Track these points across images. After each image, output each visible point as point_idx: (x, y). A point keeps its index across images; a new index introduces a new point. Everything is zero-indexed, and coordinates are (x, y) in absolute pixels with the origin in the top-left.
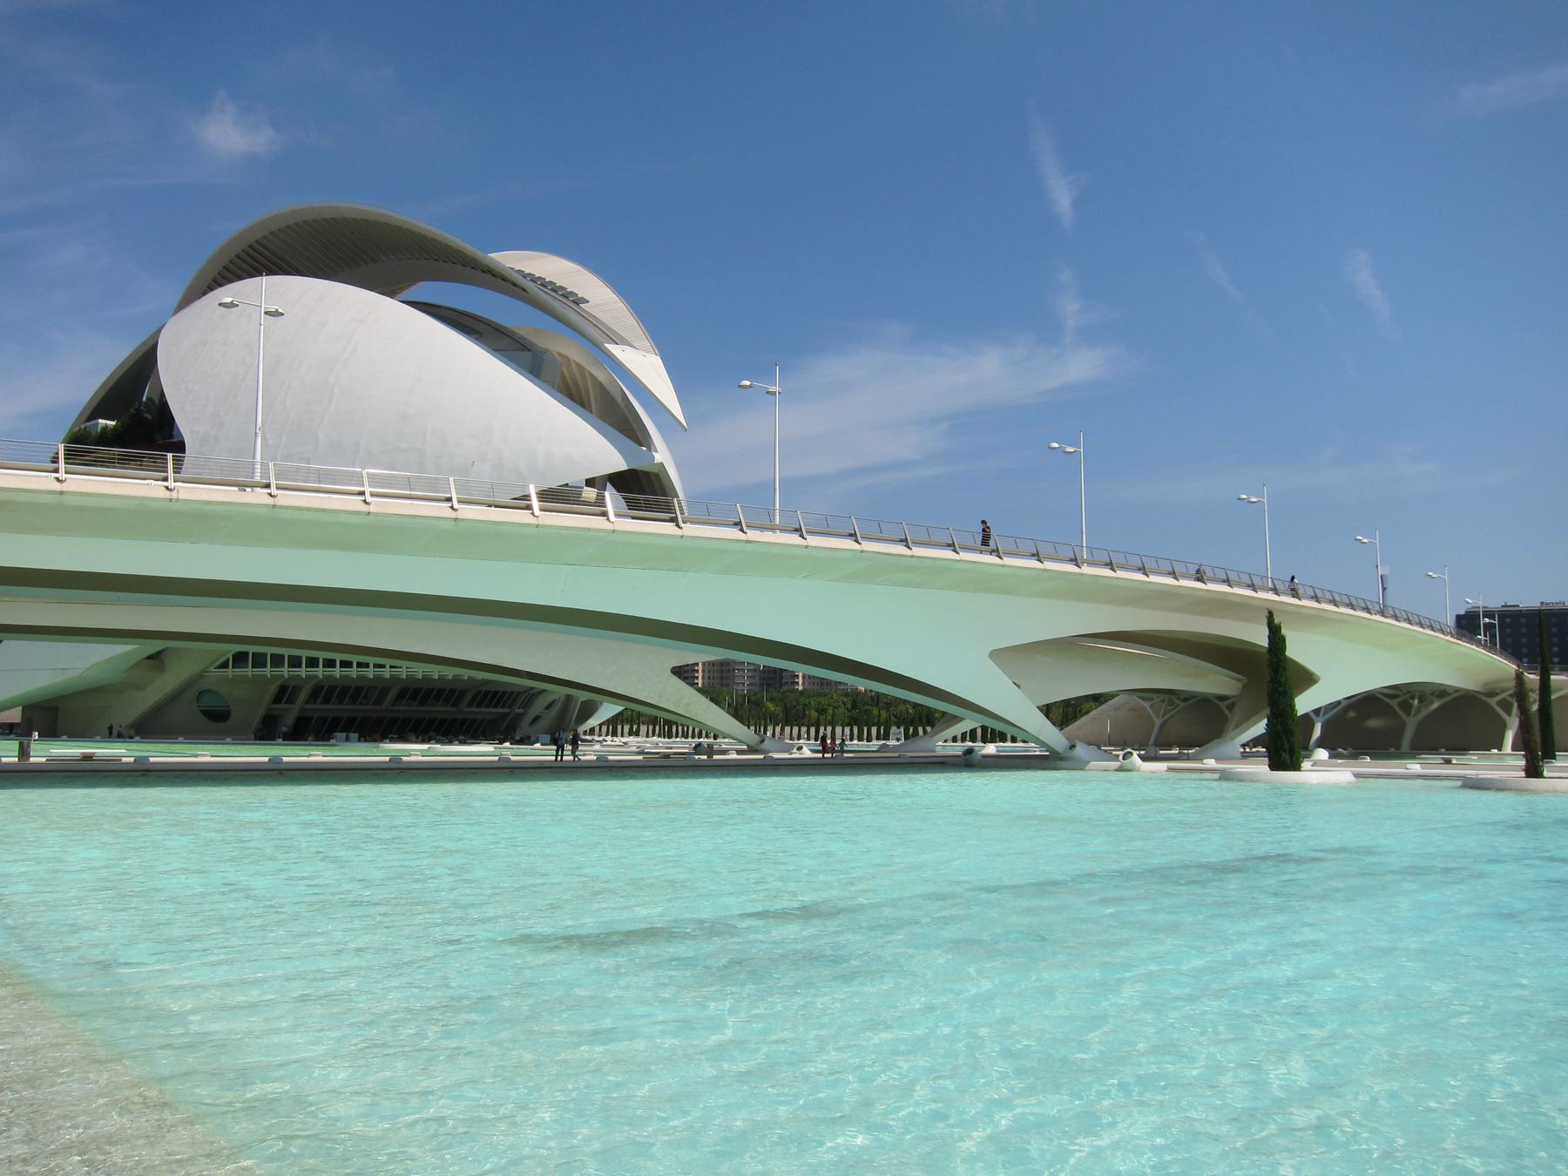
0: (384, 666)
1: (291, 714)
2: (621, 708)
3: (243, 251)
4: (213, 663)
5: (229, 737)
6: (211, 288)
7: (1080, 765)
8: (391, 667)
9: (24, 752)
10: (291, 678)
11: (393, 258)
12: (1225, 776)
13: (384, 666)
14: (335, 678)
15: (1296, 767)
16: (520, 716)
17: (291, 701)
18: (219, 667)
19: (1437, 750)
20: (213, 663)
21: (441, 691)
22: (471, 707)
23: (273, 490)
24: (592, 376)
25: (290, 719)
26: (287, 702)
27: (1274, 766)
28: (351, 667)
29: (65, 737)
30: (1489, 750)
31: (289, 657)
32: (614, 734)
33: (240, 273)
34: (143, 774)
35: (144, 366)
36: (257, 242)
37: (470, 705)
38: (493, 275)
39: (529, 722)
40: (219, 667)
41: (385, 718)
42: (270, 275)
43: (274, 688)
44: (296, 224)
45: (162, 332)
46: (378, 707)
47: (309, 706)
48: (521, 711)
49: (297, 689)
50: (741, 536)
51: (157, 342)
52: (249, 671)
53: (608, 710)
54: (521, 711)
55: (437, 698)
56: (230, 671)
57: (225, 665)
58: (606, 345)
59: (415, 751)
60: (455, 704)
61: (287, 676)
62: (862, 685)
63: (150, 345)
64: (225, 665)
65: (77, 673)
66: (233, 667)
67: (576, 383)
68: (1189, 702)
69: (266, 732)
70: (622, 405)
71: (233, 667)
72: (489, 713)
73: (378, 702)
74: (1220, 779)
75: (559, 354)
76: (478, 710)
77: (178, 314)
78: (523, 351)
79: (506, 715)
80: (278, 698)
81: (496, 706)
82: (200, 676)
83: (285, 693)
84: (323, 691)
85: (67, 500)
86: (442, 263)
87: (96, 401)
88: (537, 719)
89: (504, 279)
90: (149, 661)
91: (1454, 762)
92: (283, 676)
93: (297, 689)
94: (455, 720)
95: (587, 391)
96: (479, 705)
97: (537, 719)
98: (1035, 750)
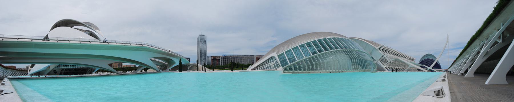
1: (63, 72)
2: (99, 69)
7: (160, 73)
9: (39, 77)
15: (181, 71)
17: (63, 71)
21: (67, 69)
25: (63, 73)
27: (180, 71)
32: (102, 73)
34: (362, 39)
38: (448, 38)
42: (495, 42)
43: (61, 70)
49: (64, 70)
50: (137, 45)
53: (97, 69)
56: (57, 68)
57: (56, 67)
59: (69, 76)
64: (56, 67)
69: (61, 74)
82: (53, 69)
83: (62, 70)
85: (70, 44)
89: (83, 24)
93: (64, 70)
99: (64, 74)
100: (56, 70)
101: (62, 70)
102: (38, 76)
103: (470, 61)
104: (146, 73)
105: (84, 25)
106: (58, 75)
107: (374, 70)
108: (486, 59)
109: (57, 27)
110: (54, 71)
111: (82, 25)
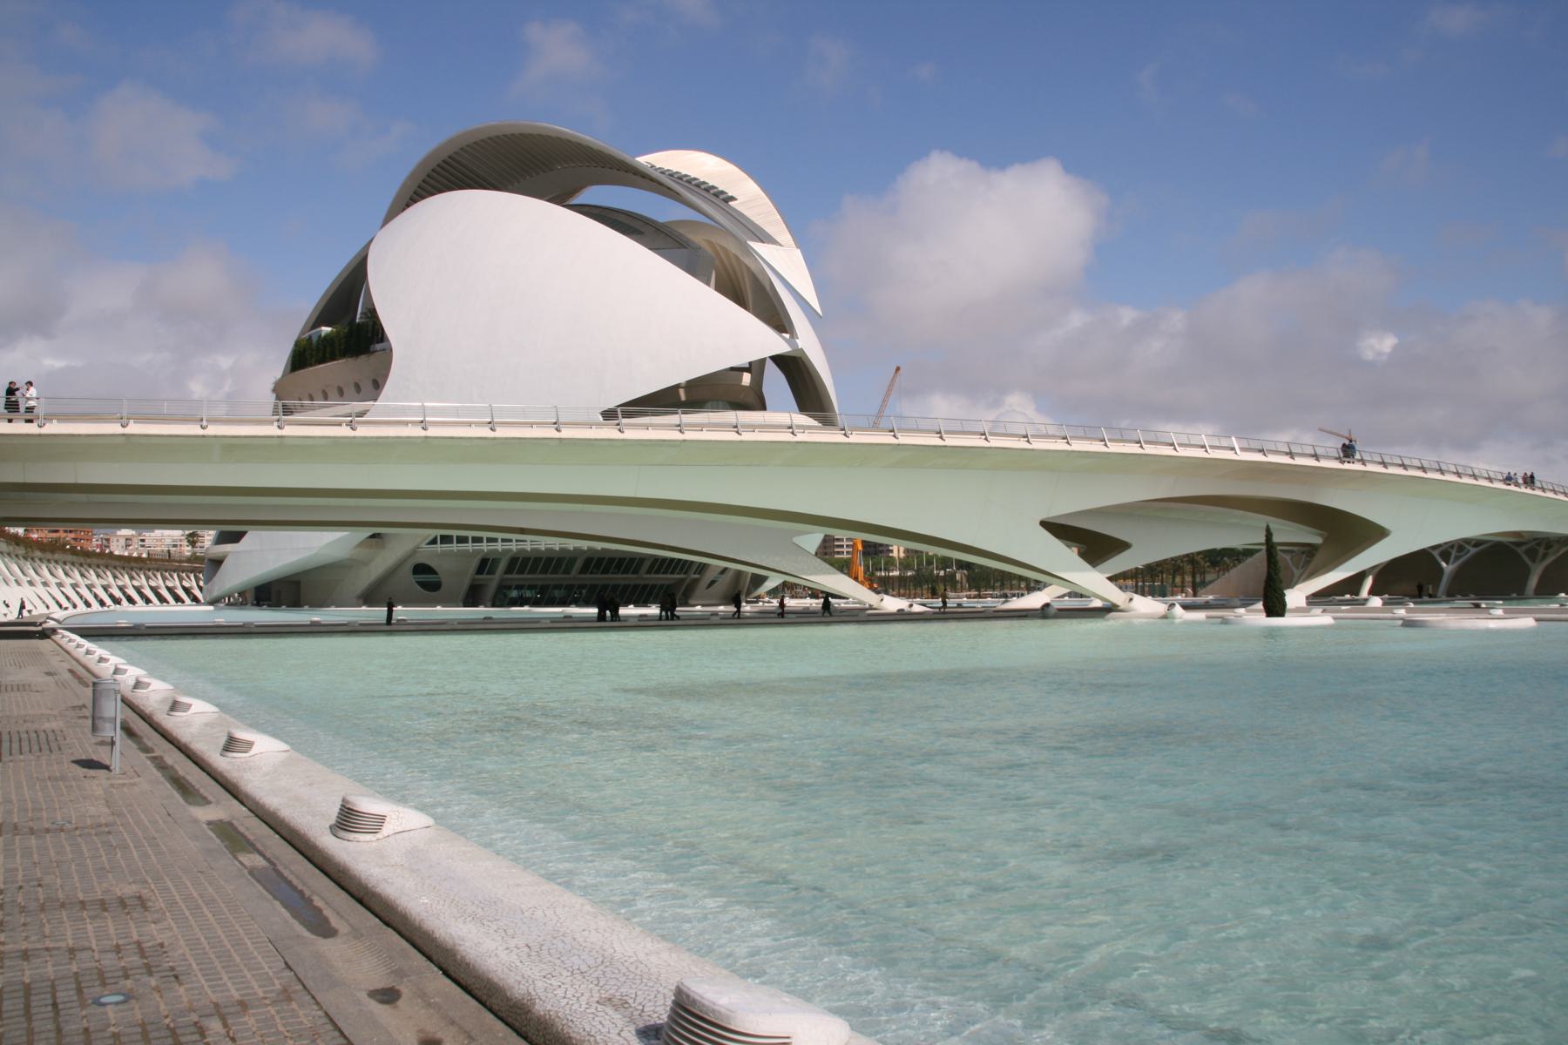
0: (510, 541)
1: (493, 582)
3: (438, 165)
4: (424, 540)
5: (1513, 593)
6: (408, 206)
8: (517, 541)
10: (490, 552)
11: (573, 165)
12: (1408, 624)
13: (510, 541)
14: (527, 551)
16: (696, 581)
17: (491, 572)
18: (428, 544)
19: (1467, 596)
20: (424, 540)
21: (550, 560)
22: (585, 573)
23: (204, 423)
24: (748, 268)
26: (487, 574)
28: (467, 542)
29: (306, 607)
30: (1343, 596)
31: (457, 537)
33: (442, 187)
35: (354, 280)
36: (450, 157)
37: (649, 572)
39: (706, 586)
40: (428, 544)
41: (629, 586)
43: (475, 563)
44: (483, 141)
45: (371, 247)
46: (568, 576)
47: (506, 576)
48: (697, 576)
49: (496, 561)
51: (367, 256)
52: (454, 547)
54: (697, 576)
55: (618, 567)
58: (748, 242)
60: (635, 572)
61: (486, 550)
62: (933, 550)
63: (363, 256)
65: (314, 551)
66: (441, 543)
67: (734, 271)
68: (1481, 547)
69: (472, 599)
70: (771, 293)
71: (441, 543)
72: (658, 578)
73: (567, 571)
74: (1222, 623)
75: (721, 246)
76: (657, 576)
77: (388, 225)
78: (679, 248)
79: (682, 580)
80: (480, 570)
81: (672, 573)
82: (414, 552)
83: (486, 565)
84: (520, 563)
86: (600, 168)
87: (320, 308)
88: (713, 582)
89: (652, 179)
90: (374, 540)
91: (1483, 606)
92: (483, 550)
93: (496, 561)
94: (636, 587)
95: (743, 279)
96: (657, 572)
97: (713, 582)
98: (1097, 603)
99: (501, 600)
100: (432, 563)
101: (484, 562)
102: (379, 612)
103: (311, 324)
104: (737, 620)
105: (661, 184)
106: (447, 601)
107: (544, 1036)
108: (31, 494)
109: (441, 191)
110: (421, 569)
111: (638, 178)
